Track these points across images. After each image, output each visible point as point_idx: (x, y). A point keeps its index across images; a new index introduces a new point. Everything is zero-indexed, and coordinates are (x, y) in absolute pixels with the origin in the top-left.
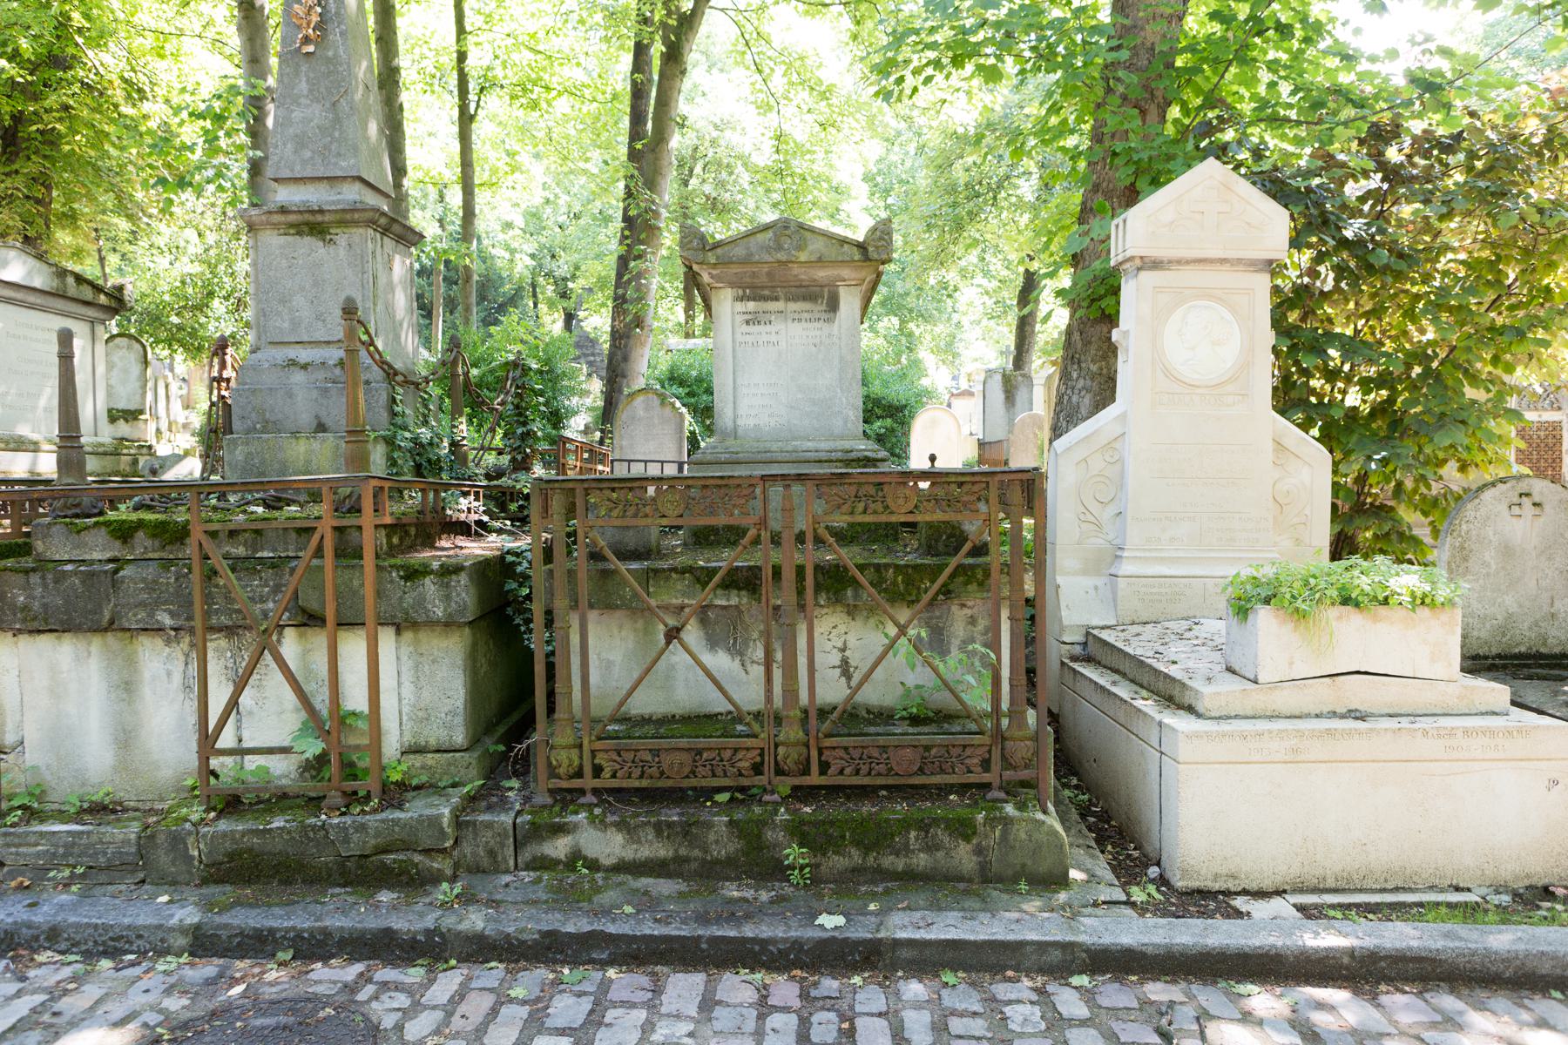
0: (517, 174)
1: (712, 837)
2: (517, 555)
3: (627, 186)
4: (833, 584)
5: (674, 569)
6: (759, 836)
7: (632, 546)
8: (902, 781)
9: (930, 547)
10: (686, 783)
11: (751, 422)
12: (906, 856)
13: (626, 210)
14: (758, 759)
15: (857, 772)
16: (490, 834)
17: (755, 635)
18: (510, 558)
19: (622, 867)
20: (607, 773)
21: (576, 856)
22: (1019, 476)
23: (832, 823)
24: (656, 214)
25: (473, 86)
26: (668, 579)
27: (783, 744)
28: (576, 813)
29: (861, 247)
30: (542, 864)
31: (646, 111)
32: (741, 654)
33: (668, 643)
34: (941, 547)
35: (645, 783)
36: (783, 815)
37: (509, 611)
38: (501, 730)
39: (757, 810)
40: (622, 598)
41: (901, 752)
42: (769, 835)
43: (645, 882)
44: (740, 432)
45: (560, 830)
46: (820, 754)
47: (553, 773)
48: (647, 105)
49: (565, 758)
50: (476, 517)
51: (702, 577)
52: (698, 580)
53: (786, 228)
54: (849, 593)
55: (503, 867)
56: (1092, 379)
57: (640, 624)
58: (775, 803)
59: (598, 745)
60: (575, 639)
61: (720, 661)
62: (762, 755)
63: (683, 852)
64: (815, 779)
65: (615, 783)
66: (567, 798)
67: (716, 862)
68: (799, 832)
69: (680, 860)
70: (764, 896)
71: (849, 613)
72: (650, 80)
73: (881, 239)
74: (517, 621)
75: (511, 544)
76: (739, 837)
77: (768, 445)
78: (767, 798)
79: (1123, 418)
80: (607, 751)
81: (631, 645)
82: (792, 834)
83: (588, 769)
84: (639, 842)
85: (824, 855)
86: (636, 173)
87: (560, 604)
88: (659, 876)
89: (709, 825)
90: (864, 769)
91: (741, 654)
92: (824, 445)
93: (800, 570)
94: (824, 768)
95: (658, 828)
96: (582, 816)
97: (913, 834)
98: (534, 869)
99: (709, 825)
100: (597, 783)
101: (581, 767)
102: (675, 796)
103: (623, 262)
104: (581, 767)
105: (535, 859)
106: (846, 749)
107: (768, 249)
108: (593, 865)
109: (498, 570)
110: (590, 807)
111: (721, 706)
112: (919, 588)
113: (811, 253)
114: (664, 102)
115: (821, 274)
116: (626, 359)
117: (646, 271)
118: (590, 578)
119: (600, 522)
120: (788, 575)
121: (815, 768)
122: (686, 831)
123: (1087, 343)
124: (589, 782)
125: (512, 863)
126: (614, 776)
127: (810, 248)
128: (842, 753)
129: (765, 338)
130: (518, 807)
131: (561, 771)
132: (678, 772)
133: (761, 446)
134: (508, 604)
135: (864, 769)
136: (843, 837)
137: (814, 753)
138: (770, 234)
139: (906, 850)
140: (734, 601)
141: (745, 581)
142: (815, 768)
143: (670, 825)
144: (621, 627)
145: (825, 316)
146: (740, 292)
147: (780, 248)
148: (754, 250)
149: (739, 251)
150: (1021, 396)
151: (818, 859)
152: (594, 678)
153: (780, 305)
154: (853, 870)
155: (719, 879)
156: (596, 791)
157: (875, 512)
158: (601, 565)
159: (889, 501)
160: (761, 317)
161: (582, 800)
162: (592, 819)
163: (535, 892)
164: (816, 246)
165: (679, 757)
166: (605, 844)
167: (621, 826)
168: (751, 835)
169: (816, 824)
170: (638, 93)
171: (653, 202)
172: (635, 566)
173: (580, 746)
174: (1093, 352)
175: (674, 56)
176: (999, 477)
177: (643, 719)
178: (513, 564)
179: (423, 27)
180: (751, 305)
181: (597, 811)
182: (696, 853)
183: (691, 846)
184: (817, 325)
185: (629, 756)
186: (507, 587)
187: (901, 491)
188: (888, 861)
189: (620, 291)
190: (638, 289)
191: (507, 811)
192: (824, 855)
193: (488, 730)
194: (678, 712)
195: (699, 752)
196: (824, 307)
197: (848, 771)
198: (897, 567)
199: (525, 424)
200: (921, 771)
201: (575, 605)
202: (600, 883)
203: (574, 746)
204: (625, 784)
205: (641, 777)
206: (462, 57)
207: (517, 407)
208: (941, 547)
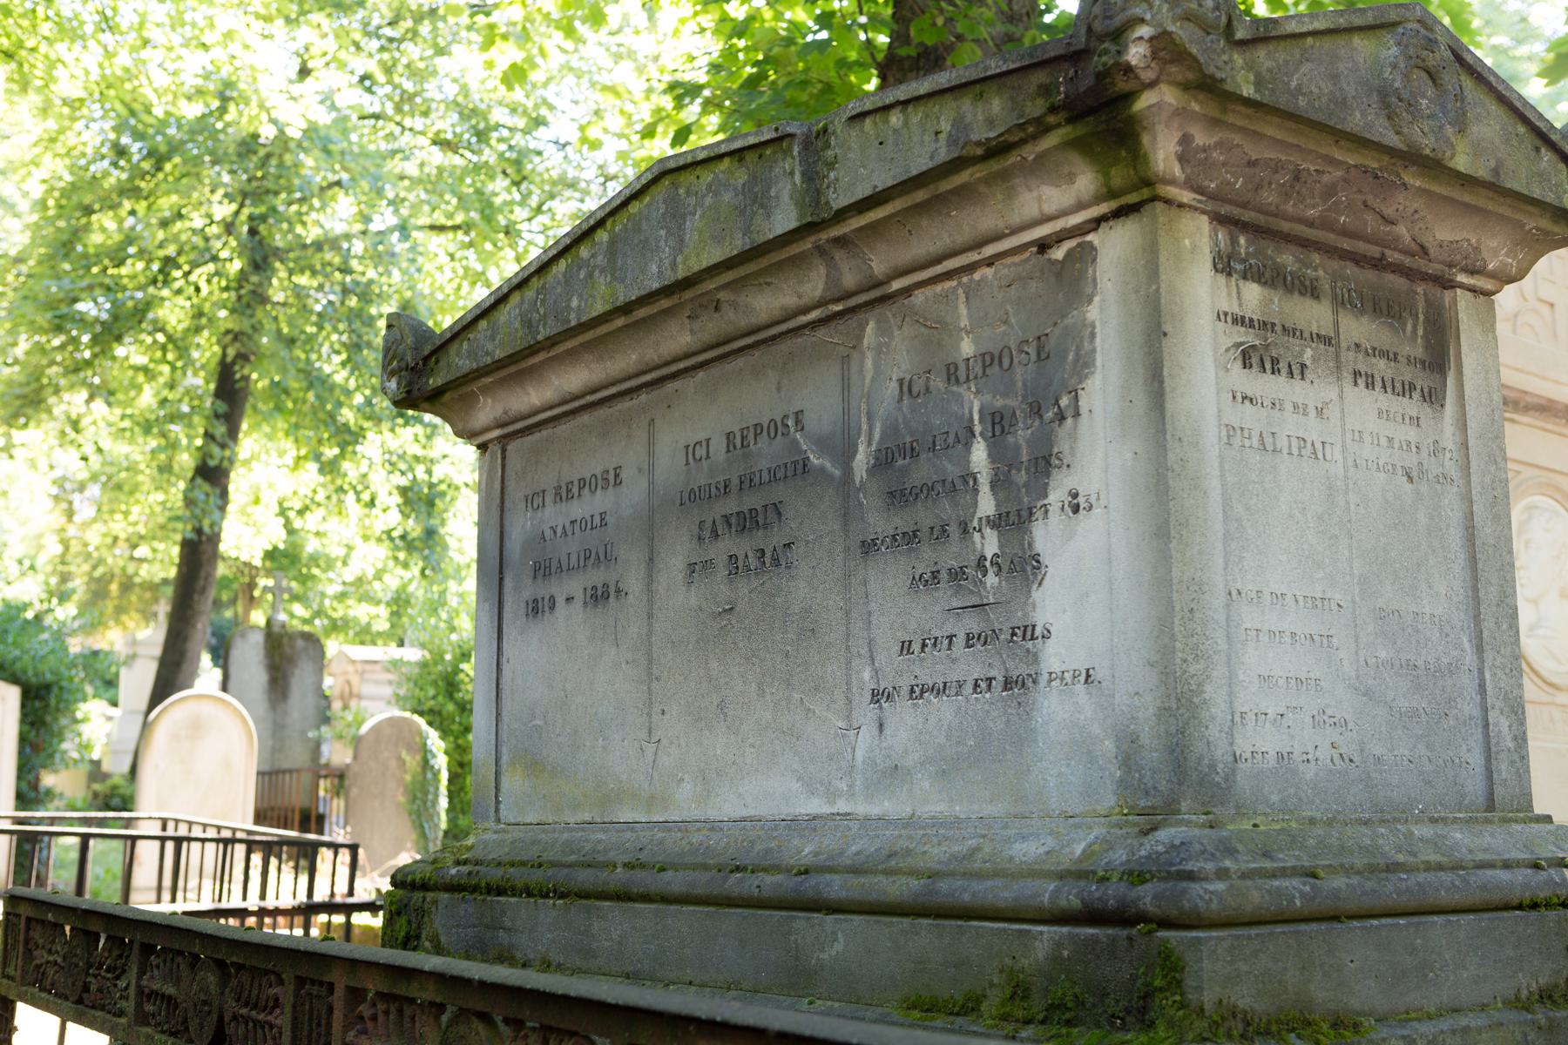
149: (1308, 81)
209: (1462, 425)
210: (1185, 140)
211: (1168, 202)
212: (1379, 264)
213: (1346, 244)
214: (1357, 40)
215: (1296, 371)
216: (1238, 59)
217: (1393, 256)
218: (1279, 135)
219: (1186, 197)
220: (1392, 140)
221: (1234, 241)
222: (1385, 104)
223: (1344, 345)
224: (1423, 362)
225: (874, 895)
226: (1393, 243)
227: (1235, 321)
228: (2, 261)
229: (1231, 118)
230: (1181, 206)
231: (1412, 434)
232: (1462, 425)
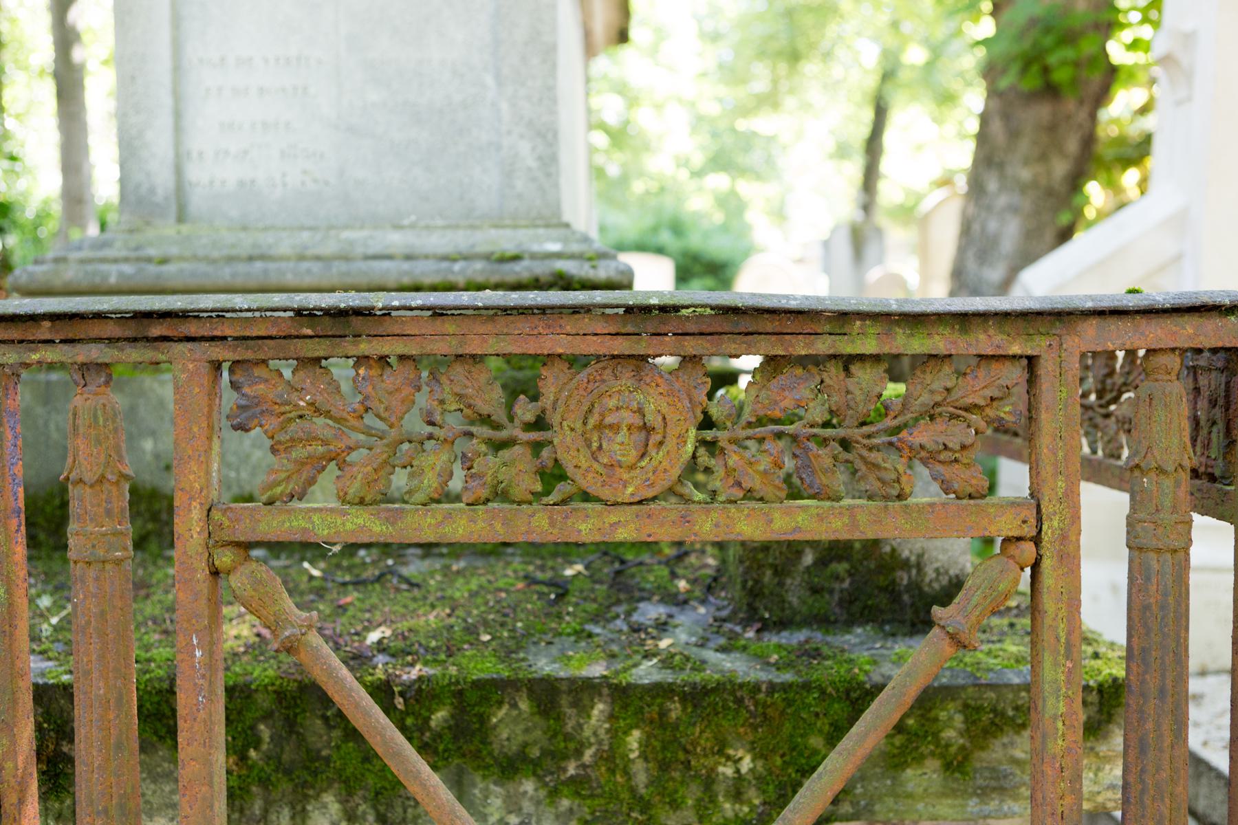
9: (754, 593)
11: (229, 174)
22: (1189, 332)
34: (795, 594)
44: (197, 202)
79: (1180, 222)
92: (439, 242)
112: (709, 782)
123: (1014, 134)
133: (246, 242)
150: (871, 251)
159: (566, 444)
176: (1090, 336)
187: (623, 398)
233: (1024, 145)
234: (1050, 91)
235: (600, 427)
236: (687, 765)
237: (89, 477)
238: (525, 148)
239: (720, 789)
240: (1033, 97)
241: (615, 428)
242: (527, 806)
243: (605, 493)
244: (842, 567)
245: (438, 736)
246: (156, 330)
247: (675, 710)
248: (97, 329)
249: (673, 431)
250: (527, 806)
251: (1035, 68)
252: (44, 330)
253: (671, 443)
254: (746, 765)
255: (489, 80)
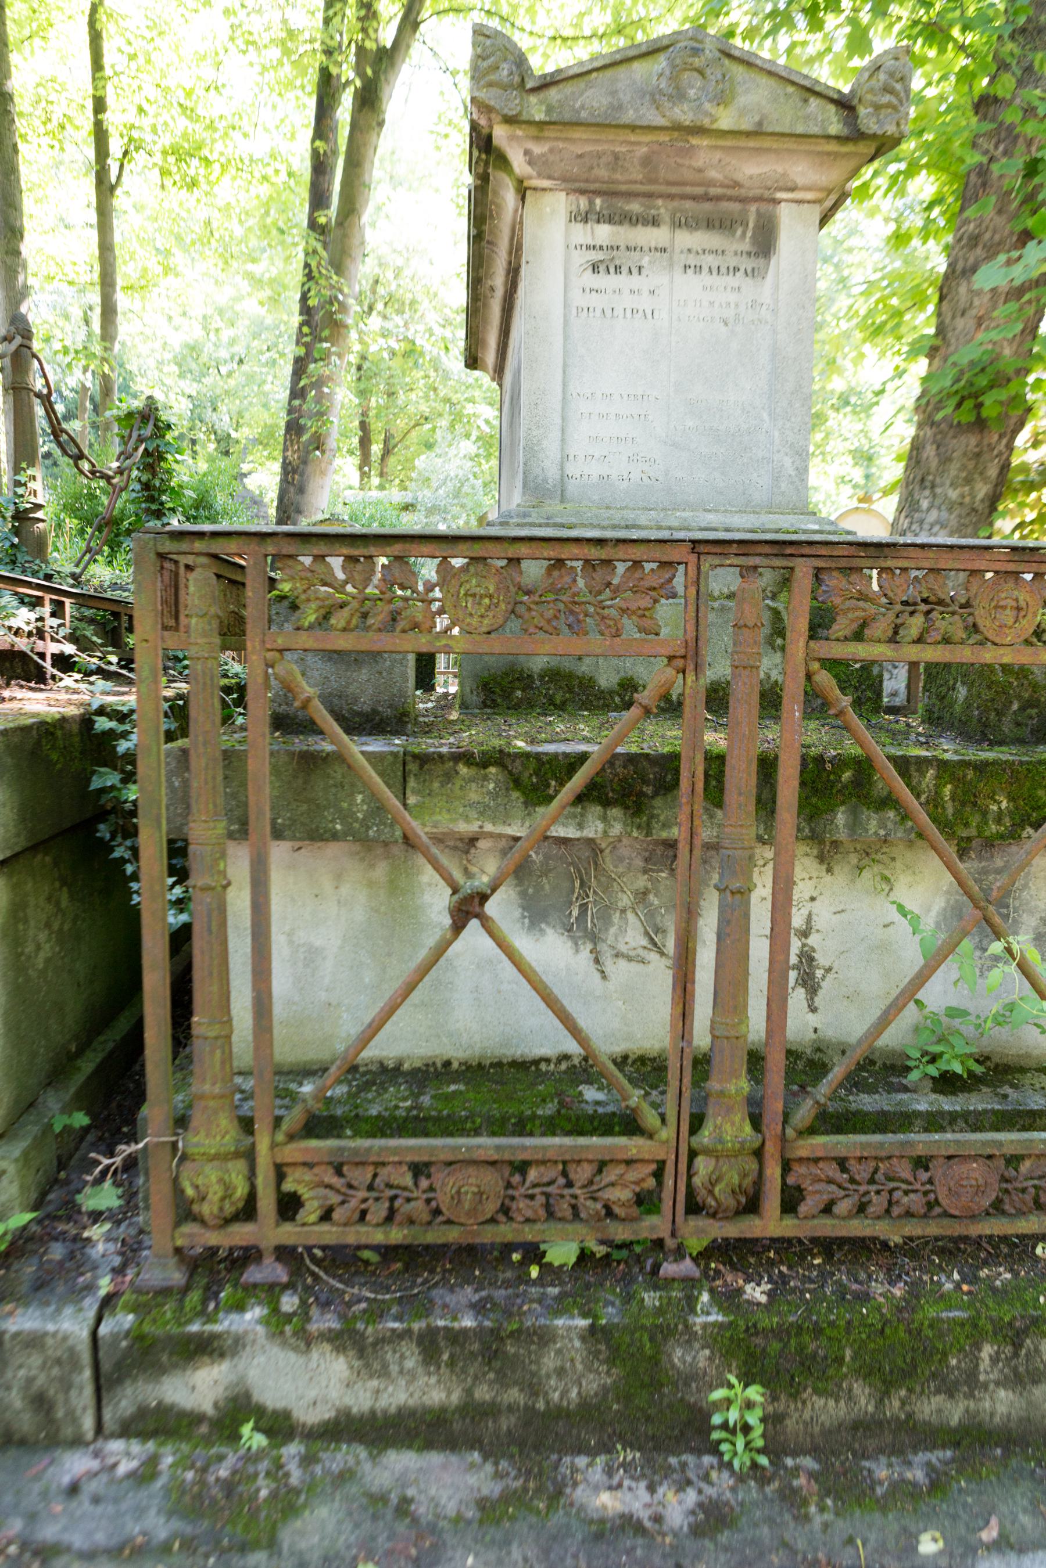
0: (171, 277)
1: (549, 1362)
2: (123, 717)
3: (307, 265)
4: (834, 800)
5: (464, 757)
6: (655, 1361)
7: (364, 703)
8: (957, 1229)
10: (490, 1235)
11: (595, 470)
12: (970, 1395)
13: (304, 298)
14: (651, 1183)
15: (861, 1209)
16: (35, 1360)
17: (625, 900)
18: (103, 724)
19: (343, 1429)
20: (310, 1212)
21: (238, 1408)
23: (817, 1331)
24: (343, 308)
25: (116, 148)
26: (449, 777)
27: (708, 1152)
28: (240, 1307)
29: (845, 105)
30: (159, 1424)
31: (329, 191)
32: (594, 938)
33: (458, 927)
34: (1007, 727)
35: (396, 1235)
36: (707, 1314)
37: (103, 831)
38: (87, 1066)
39: (651, 1298)
40: (346, 817)
41: (959, 1169)
42: (678, 1356)
43: (400, 1463)
44: (571, 487)
45: (204, 1349)
46: (786, 1167)
47: (185, 1212)
48: (331, 182)
49: (214, 1183)
50: (53, 648)
51: (535, 780)
52: (517, 783)
53: (696, 52)
54: (841, 818)
55: (68, 1432)
56: (950, 510)
57: (381, 871)
58: (689, 1283)
59: (292, 1152)
60: (239, 901)
61: (551, 951)
62: (658, 1174)
63: (483, 1393)
64: (771, 1223)
65: (329, 1234)
66: (217, 1272)
67: (557, 1413)
68: (748, 1353)
69: (475, 1412)
70: (677, 1507)
71: (821, 858)
72: (335, 152)
73: (887, 90)
74: (118, 853)
75: (100, 693)
76: (611, 1362)
77: (630, 516)
78: (669, 1269)
80: (308, 1165)
81: (360, 914)
82: (727, 1355)
83: (266, 1203)
84: (384, 1373)
85: (794, 1396)
86: (319, 247)
87: (204, 831)
88: (428, 1445)
89: (544, 1338)
90: (878, 1203)
91: (594, 938)
93: (767, 766)
94: (790, 1203)
95: (430, 1345)
96: (255, 1313)
97: (987, 1351)
98: (144, 1436)
99: (544, 1338)
100: (288, 1233)
101: (251, 1199)
102: (468, 1259)
103: (300, 366)
104: (251, 1199)
105: (142, 1412)
106: (842, 1163)
107: (655, 97)
108: (279, 1426)
109: (88, 742)
110: (272, 1291)
111: (546, 1040)
112: (985, 813)
113: (743, 112)
114: (355, 162)
115: (752, 170)
116: (301, 490)
117: (330, 378)
118: (275, 771)
119: (305, 640)
120: (742, 778)
121: (772, 1201)
122: (493, 1350)
123: (945, 460)
124: (268, 1231)
125: (88, 1423)
126: (326, 1216)
127: (742, 100)
128: (831, 1170)
129: (628, 301)
130: (105, 1285)
131: (206, 1209)
132: (473, 1212)
133: (617, 517)
134: (102, 815)
135: (878, 1203)
136: (840, 1361)
137: (773, 1171)
138: (660, 63)
139: (971, 1382)
140: (594, 829)
141: (634, 787)
142: (772, 1201)
143: (456, 1337)
144: (339, 878)
145: (747, 264)
146: (583, 202)
147: (679, 95)
148: (625, 97)
149: (592, 99)
151: (781, 1406)
152: (281, 983)
153: (659, 235)
154: (856, 1426)
155: (562, 1452)
156: (285, 1253)
157: (947, 640)
158: (299, 743)
160: (624, 258)
161: (254, 1274)
162: (277, 1321)
163: (140, 1512)
164: (754, 100)
165: (472, 1181)
166: (312, 1382)
167: (344, 1340)
168: (635, 1358)
169: (781, 1333)
170: (320, 167)
171: (341, 291)
172: (376, 745)
173: (250, 1155)
174: (953, 473)
175: (369, 100)
177: (383, 1068)
178: (111, 735)
179: (46, 74)
180: (604, 233)
181: (289, 1303)
182: (514, 1395)
183: (502, 1381)
184: (732, 281)
185: (361, 1176)
186: (96, 784)
188: (935, 1408)
189: (296, 403)
190: (319, 399)
191: (78, 1293)
192: (794, 1396)
193: (57, 1074)
194: (456, 1052)
195: (522, 1168)
196: (746, 246)
197: (842, 1207)
198: (943, 765)
199: (159, 514)
200: (997, 1208)
201: (241, 830)
202: (296, 1476)
203: (237, 1155)
204: (352, 1236)
205: (390, 1218)
206: (99, 105)
207: (147, 486)
208: (1007, 727)
209: (776, 287)
210: (527, 152)
211: (535, 189)
212: (707, 198)
213: (674, 190)
214: (636, 65)
215: (635, 271)
216: (533, 99)
217: (713, 191)
218: (584, 136)
219: (546, 183)
220: (661, 121)
221: (591, 203)
222: (654, 101)
223: (677, 250)
224: (749, 254)
225: (1013, 1052)
226: (711, 183)
227: (588, 248)
228: (389, 2)
229: (546, 134)
230: (544, 190)
231: (732, 297)
232: (776, 287)
233: (953, 469)
234: (980, 424)
235: (996, 607)
236: (975, 804)
237: (750, 624)
238: (788, 462)
239: (990, 817)
240: (960, 428)
241: (1004, 608)
242: (890, 825)
243: (997, 640)
244: (1034, 712)
245: (845, 787)
246: (788, 551)
247: (970, 774)
248: (760, 549)
249: (1031, 610)
250: (890, 825)
251: (969, 404)
252: (734, 548)
253: (1029, 616)
254: (1004, 805)
255: (765, 416)
